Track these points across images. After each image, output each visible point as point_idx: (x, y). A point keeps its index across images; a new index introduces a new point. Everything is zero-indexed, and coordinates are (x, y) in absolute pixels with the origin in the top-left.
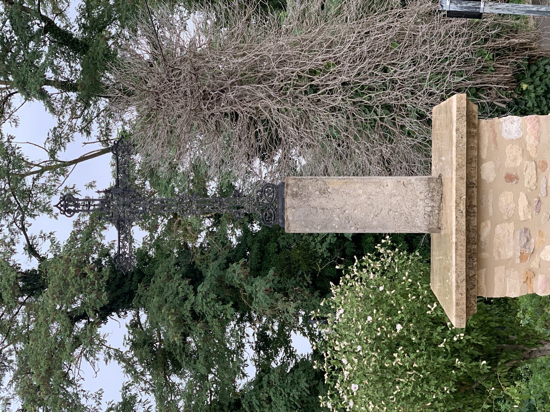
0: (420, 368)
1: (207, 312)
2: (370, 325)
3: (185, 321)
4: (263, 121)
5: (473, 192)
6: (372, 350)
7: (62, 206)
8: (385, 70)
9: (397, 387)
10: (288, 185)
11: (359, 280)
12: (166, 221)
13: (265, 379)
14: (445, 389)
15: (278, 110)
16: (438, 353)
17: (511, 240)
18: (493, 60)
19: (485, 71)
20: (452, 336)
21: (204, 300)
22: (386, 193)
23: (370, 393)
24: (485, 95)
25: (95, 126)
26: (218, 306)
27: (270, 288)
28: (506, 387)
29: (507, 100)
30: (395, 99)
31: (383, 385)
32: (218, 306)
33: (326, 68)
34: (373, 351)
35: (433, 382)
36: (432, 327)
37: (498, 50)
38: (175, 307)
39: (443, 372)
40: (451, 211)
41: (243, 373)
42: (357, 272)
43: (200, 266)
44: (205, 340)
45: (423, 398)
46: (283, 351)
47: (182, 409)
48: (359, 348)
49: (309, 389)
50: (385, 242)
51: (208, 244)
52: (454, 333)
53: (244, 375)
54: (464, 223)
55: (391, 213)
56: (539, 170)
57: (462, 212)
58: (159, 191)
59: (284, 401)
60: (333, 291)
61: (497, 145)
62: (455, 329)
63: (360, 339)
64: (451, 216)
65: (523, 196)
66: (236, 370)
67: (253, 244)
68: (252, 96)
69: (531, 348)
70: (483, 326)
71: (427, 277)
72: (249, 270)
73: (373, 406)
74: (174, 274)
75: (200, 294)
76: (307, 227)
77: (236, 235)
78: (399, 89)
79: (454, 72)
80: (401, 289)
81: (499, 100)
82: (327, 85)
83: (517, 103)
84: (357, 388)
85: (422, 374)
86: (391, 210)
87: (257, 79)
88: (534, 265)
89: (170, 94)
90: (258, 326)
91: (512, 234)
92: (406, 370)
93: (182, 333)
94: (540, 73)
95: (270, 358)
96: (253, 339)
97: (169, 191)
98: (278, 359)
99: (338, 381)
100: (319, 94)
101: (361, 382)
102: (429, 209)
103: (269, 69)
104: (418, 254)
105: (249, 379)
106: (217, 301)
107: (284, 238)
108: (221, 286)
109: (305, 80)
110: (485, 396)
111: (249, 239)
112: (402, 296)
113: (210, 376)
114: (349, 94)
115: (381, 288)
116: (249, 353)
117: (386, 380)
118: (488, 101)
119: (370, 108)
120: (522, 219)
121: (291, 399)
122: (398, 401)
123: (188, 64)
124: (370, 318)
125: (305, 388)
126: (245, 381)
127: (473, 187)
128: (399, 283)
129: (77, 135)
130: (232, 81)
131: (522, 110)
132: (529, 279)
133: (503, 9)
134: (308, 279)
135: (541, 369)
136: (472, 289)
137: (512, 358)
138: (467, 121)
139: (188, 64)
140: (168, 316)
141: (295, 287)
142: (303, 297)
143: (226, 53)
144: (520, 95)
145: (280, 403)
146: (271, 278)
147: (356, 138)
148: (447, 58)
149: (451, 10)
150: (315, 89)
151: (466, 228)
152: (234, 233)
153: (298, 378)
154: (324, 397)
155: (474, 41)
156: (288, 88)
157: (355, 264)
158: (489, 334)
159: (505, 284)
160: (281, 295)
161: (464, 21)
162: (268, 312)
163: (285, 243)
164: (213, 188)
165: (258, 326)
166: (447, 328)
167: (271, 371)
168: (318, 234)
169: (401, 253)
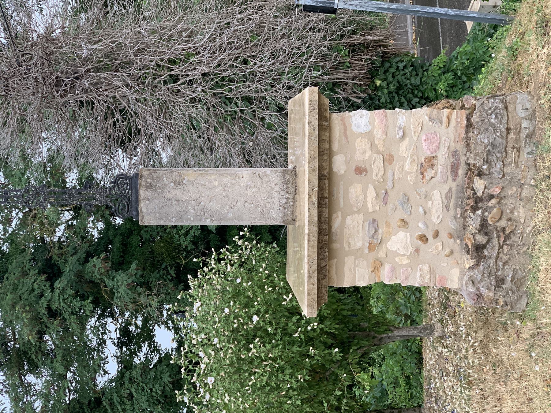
0: (276, 358)
1: (65, 309)
2: (227, 317)
3: (41, 319)
4: (121, 111)
5: (325, 184)
8: (245, 62)
9: (253, 378)
10: (141, 176)
11: (217, 273)
12: (21, 215)
13: (127, 375)
14: (299, 378)
15: (136, 99)
16: (293, 343)
17: (360, 231)
18: (349, 56)
19: (341, 66)
20: (307, 325)
21: (62, 297)
22: (242, 185)
23: (226, 385)
24: (341, 90)
26: (77, 303)
27: (133, 282)
28: (357, 373)
29: (362, 95)
30: (255, 92)
31: (239, 376)
32: (75, 303)
33: (185, 58)
34: (230, 344)
35: (288, 371)
37: (354, 46)
38: (30, 305)
39: (298, 361)
40: (304, 203)
41: (104, 370)
43: (58, 261)
44: (62, 338)
45: (278, 388)
46: (146, 346)
47: (39, 409)
48: (216, 340)
49: (172, 383)
50: (243, 235)
51: (67, 238)
52: (308, 322)
53: (105, 372)
54: (316, 215)
55: (246, 205)
56: (386, 163)
57: (314, 204)
58: (13, 182)
59: (146, 397)
60: (190, 284)
61: (347, 138)
62: (309, 319)
63: (217, 332)
64: (304, 207)
65: (371, 188)
66: (97, 368)
67: (115, 237)
68: (109, 84)
69: (381, 334)
70: (337, 316)
72: (110, 264)
73: (229, 398)
74: (29, 270)
75: (58, 290)
76: (161, 219)
77: (97, 228)
78: (258, 81)
79: (312, 67)
80: (258, 280)
81: (354, 95)
82: (187, 76)
83: (371, 99)
84: (213, 381)
85: (278, 364)
86: (246, 202)
87: (114, 67)
89: (20, 80)
90: (120, 321)
91: (361, 224)
92: (262, 361)
93: (37, 331)
94: (392, 70)
95: (133, 354)
96: (115, 335)
97: (23, 183)
98: (141, 355)
99: (195, 374)
100: (179, 85)
101: (218, 375)
102: (284, 201)
103: (127, 56)
104: (275, 246)
105: (110, 376)
106: (75, 297)
107: (147, 231)
108: (81, 282)
109: (165, 69)
110: (338, 382)
111: (111, 233)
113: (69, 375)
114: (209, 85)
115: (239, 281)
116: (111, 350)
117: (242, 372)
118: (344, 96)
119: (230, 100)
120: (371, 210)
121: (154, 394)
122: (254, 392)
123: (39, 48)
124: (227, 310)
125: (168, 383)
126: (106, 378)
127: (325, 179)
128: (256, 275)
130: (86, 68)
131: (376, 105)
132: (376, 268)
133: (356, 5)
134: (172, 272)
135: (392, 355)
137: (363, 345)
138: (319, 114)
139: (39, 48)
140: (22, 314)
141: (159, 281)
142: (167, 291)
143: (81, 38)
144: (374, 91)
145: (142, 400)
147: (215, 129)
148: (304, 52)
149: (307, 4)
150: (174, 79)
151: (318, 219)
152: (95, 227)
153: (161, 373)
154: (180, 392)
155: (331, 36)
156: (146, 77)
157: (213, 256)
158: (341, 322)
159: (354, 274)
160: (144, 289)
161: (322, 16)
162: (130, 306)
163: (149, 236)
164: (73, 179)
165: (120, 321)
166: (301, 318)
167: (133, 367)
168: (182, 226)
169: (259, 245)
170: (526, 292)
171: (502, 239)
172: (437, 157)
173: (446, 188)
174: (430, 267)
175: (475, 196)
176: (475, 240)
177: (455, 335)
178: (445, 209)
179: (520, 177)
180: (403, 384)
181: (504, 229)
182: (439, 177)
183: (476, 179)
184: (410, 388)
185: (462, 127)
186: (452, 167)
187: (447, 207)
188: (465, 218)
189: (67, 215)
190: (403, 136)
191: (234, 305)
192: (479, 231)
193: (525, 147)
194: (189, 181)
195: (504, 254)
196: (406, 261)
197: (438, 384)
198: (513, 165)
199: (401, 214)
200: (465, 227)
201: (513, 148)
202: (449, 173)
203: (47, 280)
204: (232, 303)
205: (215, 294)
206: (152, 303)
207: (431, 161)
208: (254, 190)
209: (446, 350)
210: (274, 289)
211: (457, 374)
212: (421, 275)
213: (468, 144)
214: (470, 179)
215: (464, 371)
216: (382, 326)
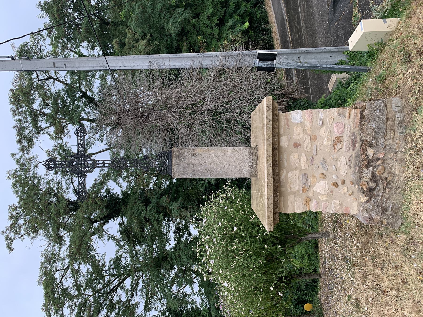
5: (276, 153)
6: (221, 240)
7: (47, 165)
10: (173, 152)
17: (297, 180)
25: (105, 138)
26: (156, 215)
35: (253, 258)
36: (252, 228)
37: (279, 95)
42: (214, 199)
53: (170, 244)
54: (272, 171)
55: (230, 166)
56: (312, 141)
61: (289, 127)
63: (215, 234)
65: (303, 155)
71: (249, 201)
76: (184, 175)
88: (310, 194)
95: (181, 236)
98: (184, 237)
102: (251, 164)
104: (244, 190)
111: (171, 186)
112: (237, 211)
115: (226, 208)
116: (172, 235)
121: (189, 255)
124: (220, 224)
127: (276, 151)
129: (97, 142)
133: (285, 65)
136: (276, 208)
146: (180, 202)
150: (194, 113)
159: (294, 206)
163: (186, 187)
170: (401, 216)
171: (385, 185)
172: (343, 136)
173: (349, 154)
174: (339, 201)
175: (368, 159)
176: (368, 185)
177: (343, 238)
178: (348, 167)
179: (395, 147)
180: (307, 258)
181: (386, 179)
182: (344, 148)
183: (368, 149)
184: (310, 261)
185: (357, 119)
186: (352, 142)
187: (350, 166)
188: (361, 172)
189: (155, 179)
190: (322, 125)
191: (224, 220)
192: (371, 180)
193: (398, 129)
194: (199, 154)
195: (386, 193)
196: (325, 198)
197: (331, 263)
198: (391, 140)
199: (321, 170)
200: (361, 178)
201: (391, 130)
202: (350, 146)
203: (144, 205)
204: (223, 220)
205: (214, 215)
206: (188, 215)
207: (339, 139)
208: (234, 158)
209: (336, 245)
210: (245, 212)
211: (345, 258)
212: (334, 207)
213: (362, 129)
214: (363, 149)
215: (349, 258)
216: (302, 233)
